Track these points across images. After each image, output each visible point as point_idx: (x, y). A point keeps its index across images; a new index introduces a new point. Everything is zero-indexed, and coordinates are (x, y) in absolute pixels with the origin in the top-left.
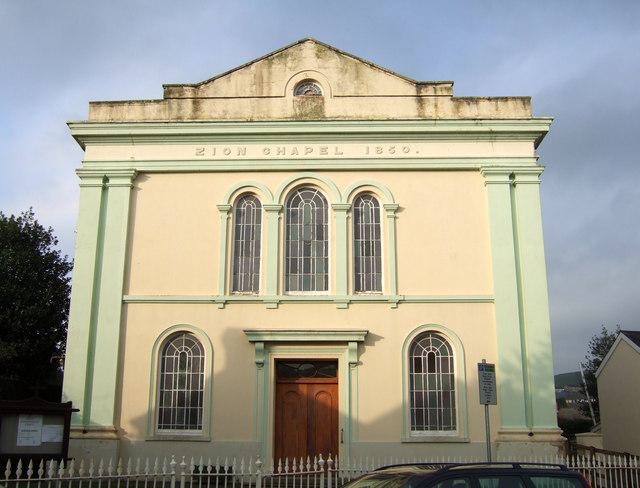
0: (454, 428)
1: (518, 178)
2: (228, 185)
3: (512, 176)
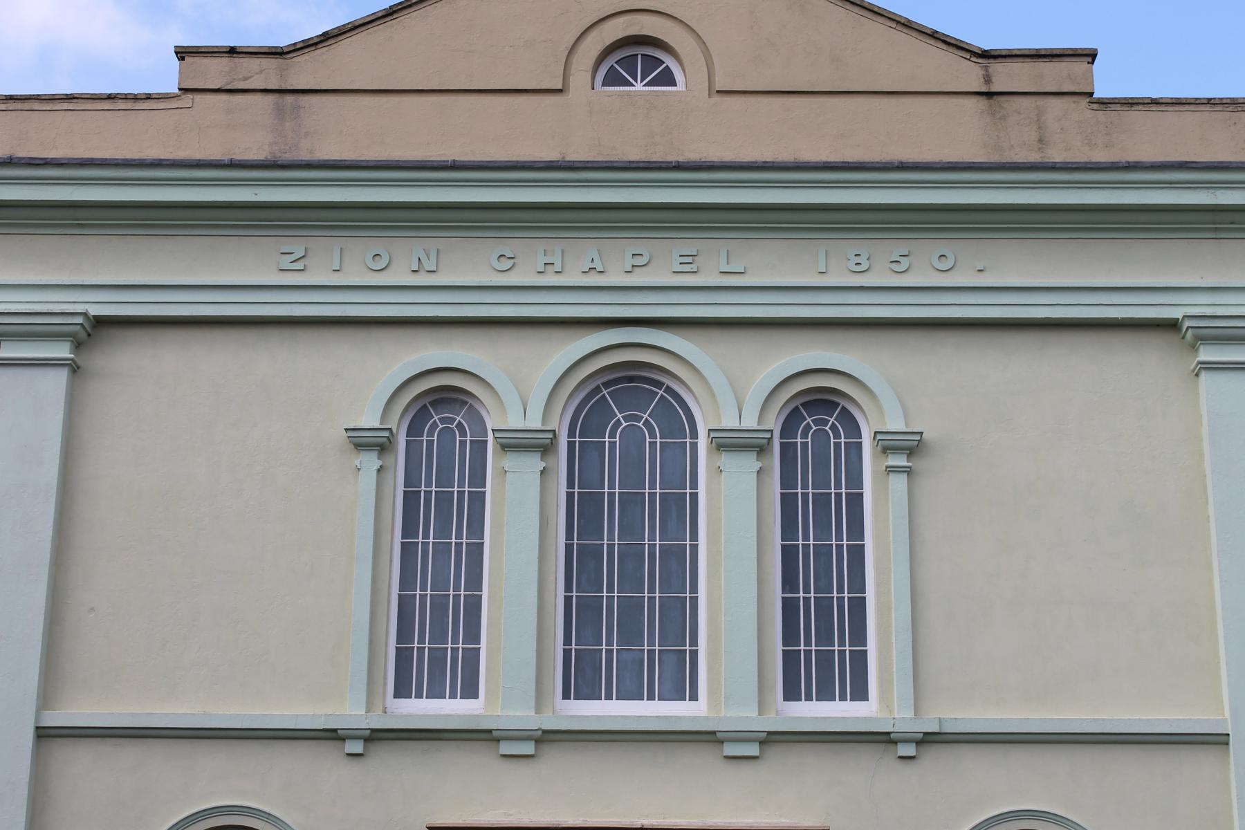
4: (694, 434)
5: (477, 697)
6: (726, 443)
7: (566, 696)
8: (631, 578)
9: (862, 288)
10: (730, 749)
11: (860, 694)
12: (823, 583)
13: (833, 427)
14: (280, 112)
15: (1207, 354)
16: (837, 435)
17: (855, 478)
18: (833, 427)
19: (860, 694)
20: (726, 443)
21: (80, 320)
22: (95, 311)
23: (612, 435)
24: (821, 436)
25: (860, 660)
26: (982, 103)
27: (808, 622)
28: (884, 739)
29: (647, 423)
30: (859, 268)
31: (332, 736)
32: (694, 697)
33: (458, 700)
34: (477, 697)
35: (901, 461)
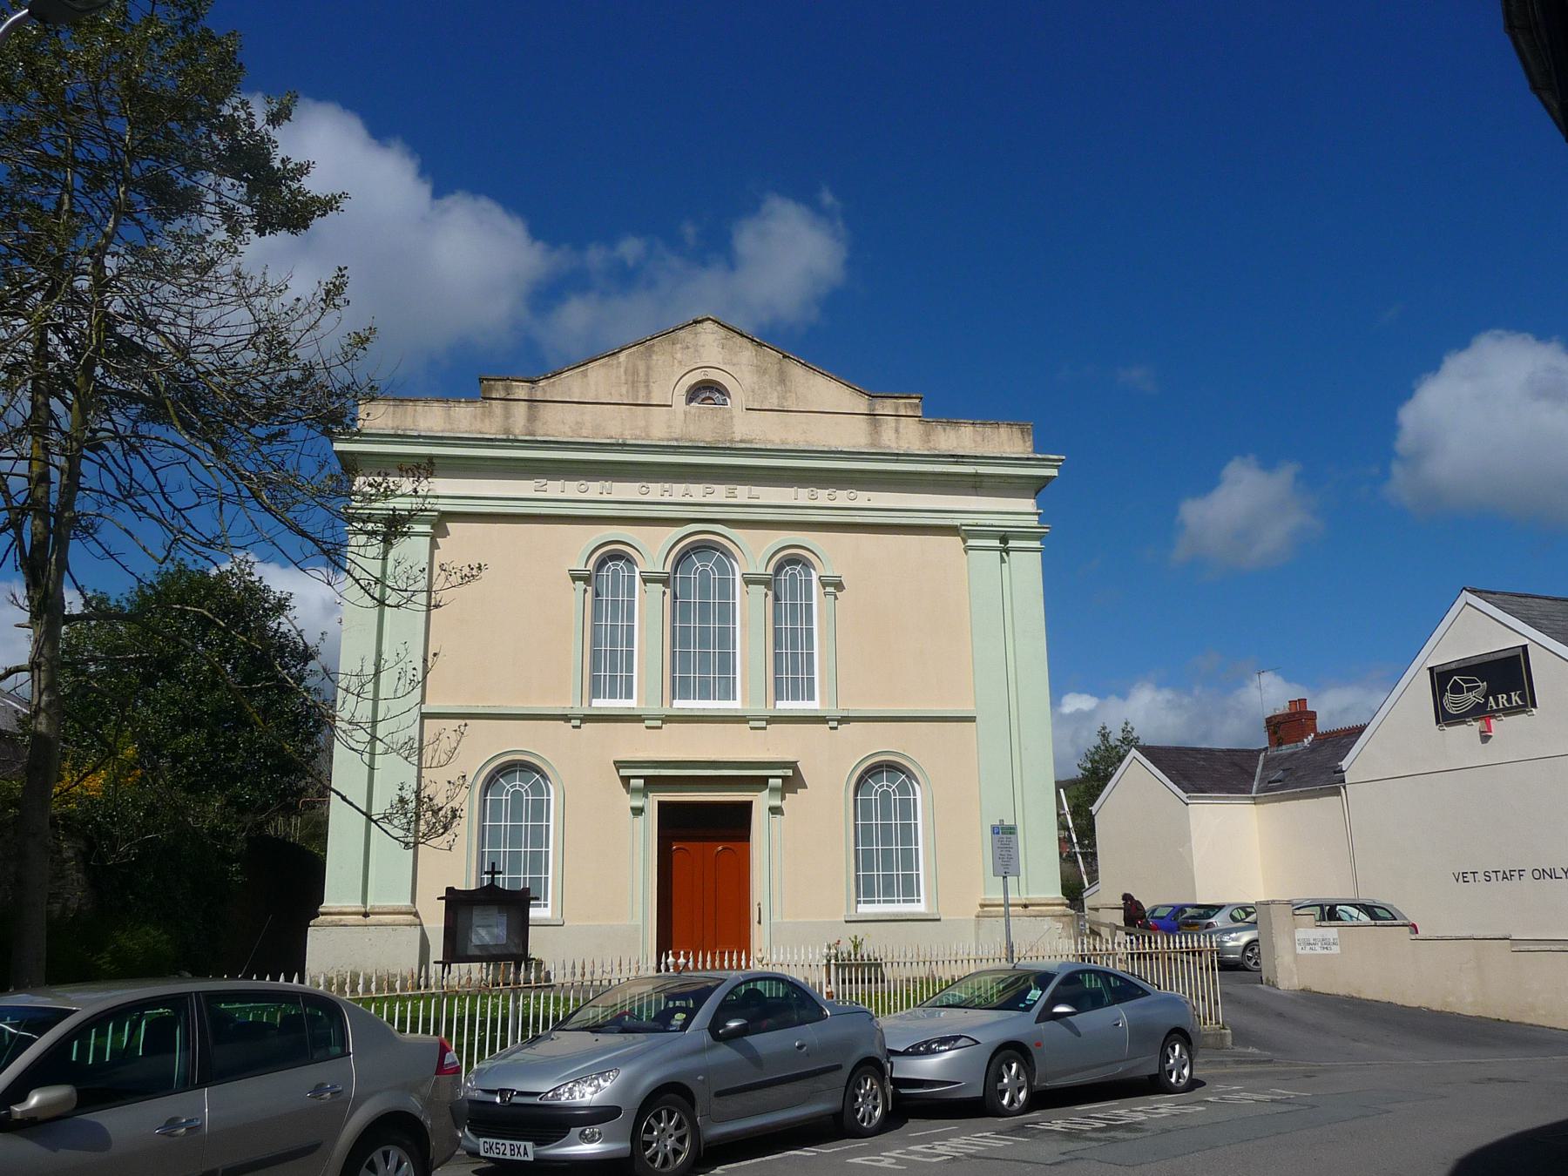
2: (580, 544)
3: (1004, 539)
4: (734, 574)
5: (632, 698)
6: (749, 581)
8: (704, 642)
9: (545, 441)
10: (753, 724)
11: (629, 695)
12: (794, 645)
13: (799, 572)
14: (530, 408)
15: (971, 542)
16: (801, 576)
17: (809, 596)
18: (799, 572)
19: (629, 695)
20: (749, 581)
21: (436, 513)
22: (442, 508)
25: (630, 679)
27: (786, 663)
28: (822, 720)
30: (813, 497)
31: (566, 718)
32: (734, 699)
33: (607, 699)
34: (632, 698)
35: (831, 589)
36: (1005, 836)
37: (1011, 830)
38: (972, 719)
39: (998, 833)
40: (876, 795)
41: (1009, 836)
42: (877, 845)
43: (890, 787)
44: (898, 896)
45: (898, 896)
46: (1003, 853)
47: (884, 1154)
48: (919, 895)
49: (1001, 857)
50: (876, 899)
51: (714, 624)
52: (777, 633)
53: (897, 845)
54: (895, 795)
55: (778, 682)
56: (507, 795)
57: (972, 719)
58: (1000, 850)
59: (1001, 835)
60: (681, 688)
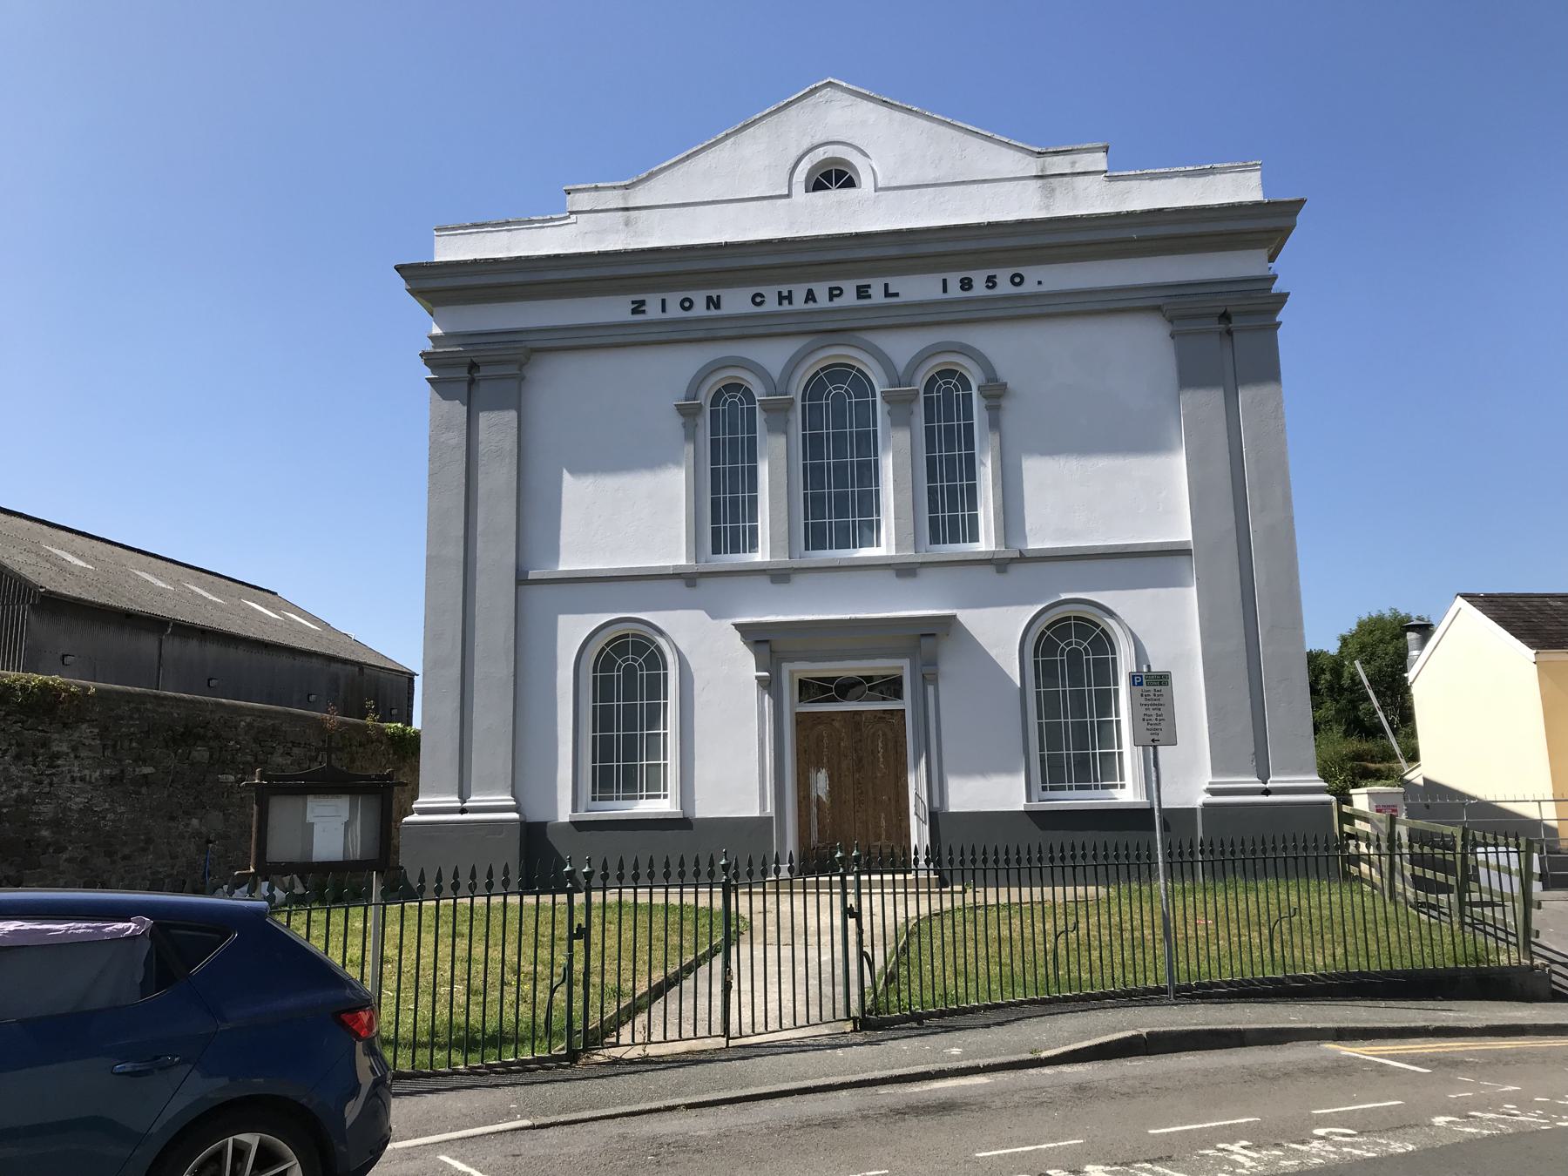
0: (1123, 786)
1: (1236, 323)
3: (1225, 317)
4: (874, 395)
7: (807, 548)
17: (969, 415)
18: (955, 385)
23: (827, 399)
24: (948, 392)
26: (1040, 182)
29: (846, 391)
32: (878, 545)
36: (1152, 688)
37: (1163, 679)
38: (1460, 609)
39: (1140, 684)
40: (1062, 655)
41: (1158, 688)
42: (1066, 717)
43: (636, 661)
44: (1070, 781)
45: (1070, 781)
46: (1148, 712)
47: (1221, 1146)
48: (1122, 779)
49: (1146, 718)
50: (1093, 783)
51: (852, 459)
52: (931, 462)
53: (1066, 717)
54: (1087, 654)
55: (933, 522)
56: (618, 671)
57: (1460, 609)
58: (1144, 707)
59: (1145, 687)
60: (816, 539)
